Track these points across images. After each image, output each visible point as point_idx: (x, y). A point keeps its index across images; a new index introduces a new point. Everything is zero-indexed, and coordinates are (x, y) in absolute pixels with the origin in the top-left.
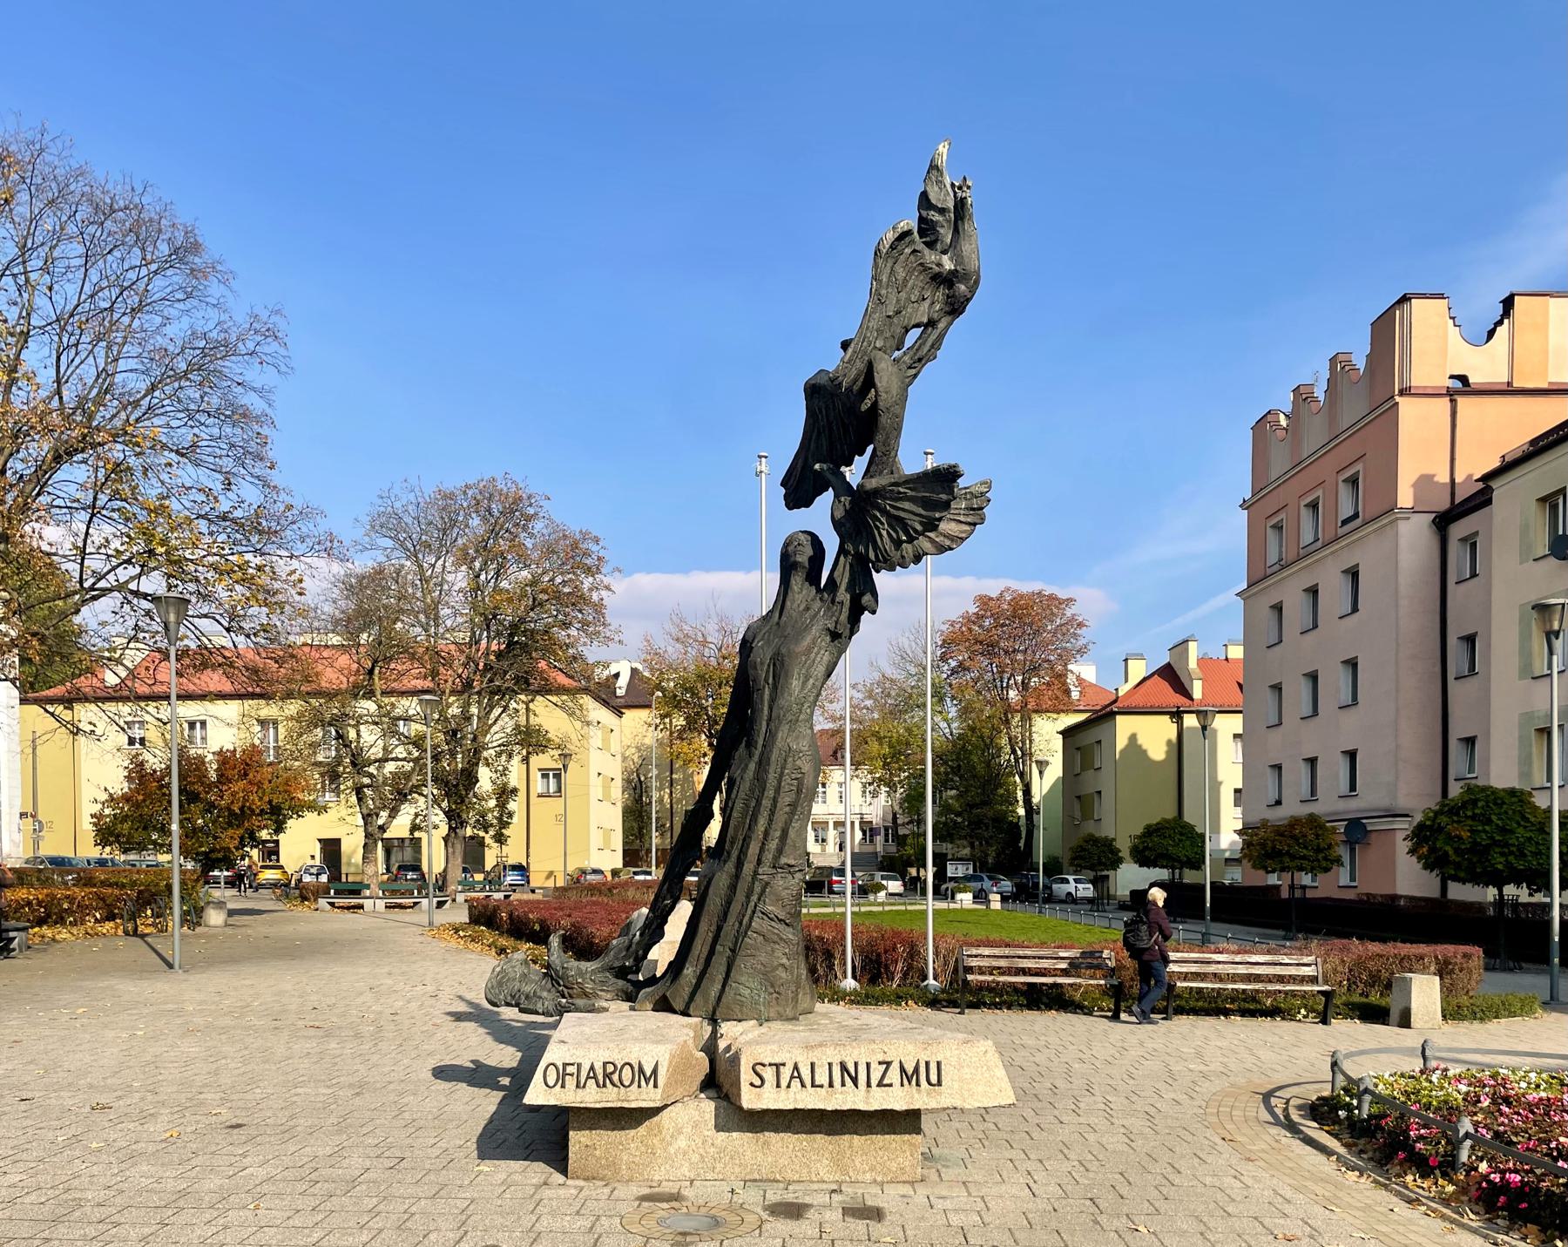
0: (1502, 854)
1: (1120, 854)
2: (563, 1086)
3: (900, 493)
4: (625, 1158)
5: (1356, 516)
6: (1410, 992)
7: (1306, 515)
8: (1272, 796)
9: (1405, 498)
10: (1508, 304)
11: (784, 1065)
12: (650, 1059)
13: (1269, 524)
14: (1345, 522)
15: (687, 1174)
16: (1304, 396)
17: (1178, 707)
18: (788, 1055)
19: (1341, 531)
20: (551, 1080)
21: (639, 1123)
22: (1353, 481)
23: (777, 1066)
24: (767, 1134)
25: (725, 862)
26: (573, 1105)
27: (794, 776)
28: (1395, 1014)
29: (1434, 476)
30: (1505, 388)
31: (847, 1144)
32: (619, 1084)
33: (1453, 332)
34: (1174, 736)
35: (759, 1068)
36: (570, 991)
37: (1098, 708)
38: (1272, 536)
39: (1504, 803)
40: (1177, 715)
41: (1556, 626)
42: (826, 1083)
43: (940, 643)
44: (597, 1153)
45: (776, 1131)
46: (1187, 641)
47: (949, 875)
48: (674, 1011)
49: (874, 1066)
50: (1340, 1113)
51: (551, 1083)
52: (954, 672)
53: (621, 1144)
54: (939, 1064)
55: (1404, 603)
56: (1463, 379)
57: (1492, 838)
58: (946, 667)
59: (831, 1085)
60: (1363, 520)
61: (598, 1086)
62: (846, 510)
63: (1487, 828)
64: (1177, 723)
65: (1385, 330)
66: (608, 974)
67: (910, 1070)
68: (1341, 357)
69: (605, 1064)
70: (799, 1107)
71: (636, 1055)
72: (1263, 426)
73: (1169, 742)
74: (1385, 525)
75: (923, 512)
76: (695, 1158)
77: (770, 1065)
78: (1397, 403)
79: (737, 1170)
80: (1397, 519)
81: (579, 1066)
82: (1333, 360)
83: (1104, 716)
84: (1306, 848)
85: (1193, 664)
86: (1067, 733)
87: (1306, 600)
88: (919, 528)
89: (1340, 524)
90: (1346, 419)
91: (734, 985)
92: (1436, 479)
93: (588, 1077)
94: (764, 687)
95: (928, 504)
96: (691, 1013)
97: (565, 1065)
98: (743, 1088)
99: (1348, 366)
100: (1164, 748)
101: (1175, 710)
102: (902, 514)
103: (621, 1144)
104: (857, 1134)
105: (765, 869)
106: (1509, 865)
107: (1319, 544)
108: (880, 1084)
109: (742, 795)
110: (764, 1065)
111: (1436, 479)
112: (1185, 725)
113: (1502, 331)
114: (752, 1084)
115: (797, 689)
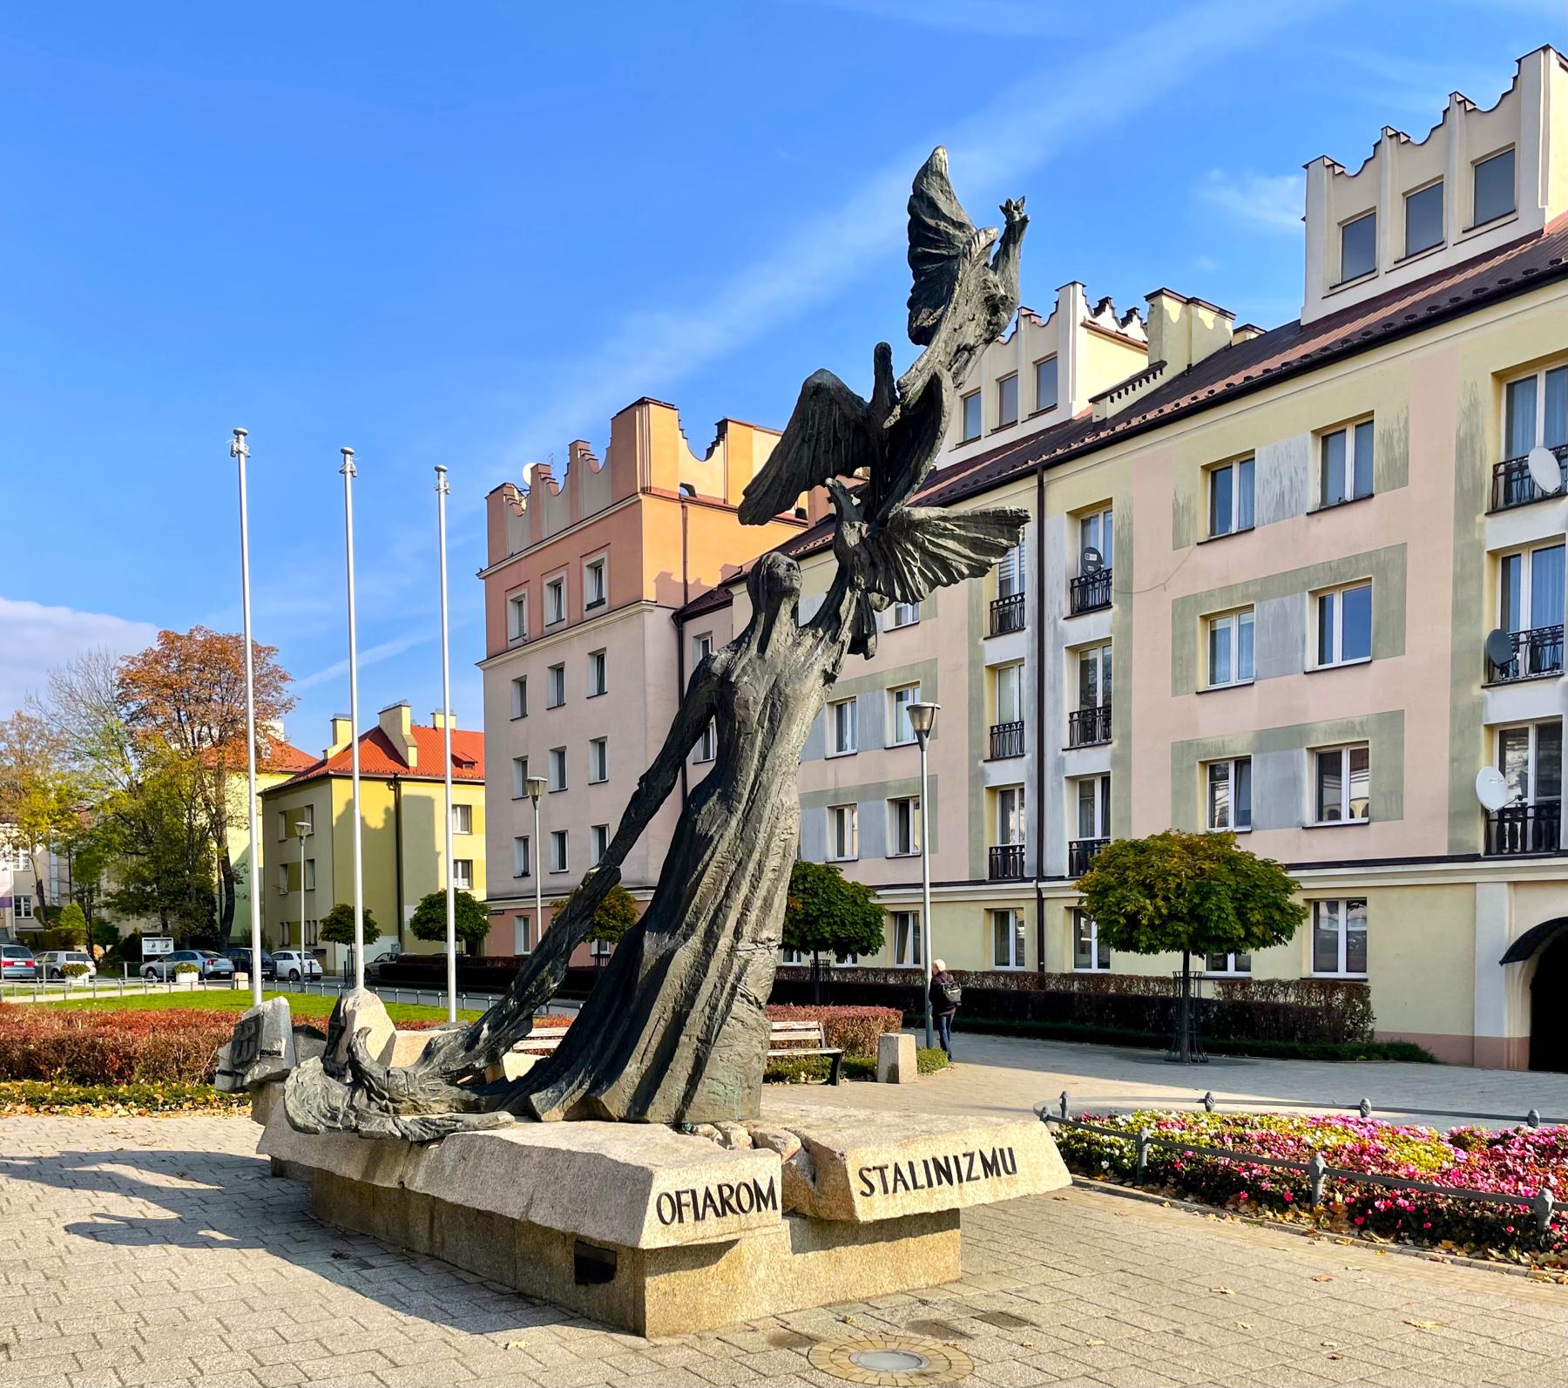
0: (829, 924)
1: (376, 927)
2: (681, 1220)
3: (946, 529)
4: (706, 1300)
5: (601, 602)
6: (897, 1051)
7: (549, 595)
8: (519, 869)
9: (649, 592)
10: (722, 426)
11: (887, 1167)
12: (764, 1176)
13: (509, 598)
14: (590, 607)
15: (768, 1308)
16: (543, 476)
17: (396, 774)
18: (887, 1156)
19: (588, 615)
20: (667, 1215)
21: (719, 1257)
22: (597, 568)
23: (882, 1169)
24: (838, 1249)
25: (686, 938)
26: (695, 1243)
27: (783, 837)
28: (882, 1072)
29: (671, 575)
30: (722, 503)
31: (904, 1249)
32: (738, 1210)
33: (683, 443)
34: (391, 804)
35: (865, 1173)
36: (397, 1105)
37: (302, 770)
38: (512, 610)
39: (825, 878)
40: (394, 782)
41: (925, 727)
42: (926, 1184)
43: (117, 682)
44: (678, 1300)
45: (846, 1244)
46: (400, 706)
47: (145, 952)
48: (610, 1119)
49: (961, 1158)
50: (1103, 1163)
51: (667, 1218)
52: (134, 717)
53: (701, 1284)
54: (1010, 1150)
55: (650, 690)
56: (690, 488)
57: (820, 910)
58: (124, 711)
59: (930, 1184)
60: (609, 607)
61: (717, 1215)
62: (861, 538)
63: (816, 900)
64: (395, 790)
65: (626, 422)
66: (439, 1081)
67: (990, 1160)
68: (581, 445)
69: (720, 1187)
70: (907, 1213)
71: (749, 1173)
72: (498, 496)
73: (387, 810)
74: (631, 615)
75: (972, 555)
76: (775, 1288)
77: (874, 1168)
78: (640, 500)
79: (814, 1295)
80: (643, 610)
81: (694, 1193)
82: (573, 446)
83: (317, 777)
84: (614, 918)
85: (406, 731)
86: (268, 796)
87: (550, 677)
88: (966, 571)
89: (585, 607)
90: (588, 508)
91: (707, 1081)
92: (673, 578)
93: (705, 1205)
94: (756, 731)
95: (975, 545)
96: (649, 1119)
97: (678, 1194)
98: (855, 1198)
99: (588, 458)
100: (383, 816)
101: (392, 776)
102: (945, 553)
103: (701, 1284)
104: (911, 1236)
105: (744, 944)
106: (833, 933)
107: (564, 624)
108: (969, 1178)
109: (718, 857)
110: (869, 1170)
111: (673, 578)
112: (403, 793)
113: (718, 450)
114: (863, 1193)
115: (796, 737)
